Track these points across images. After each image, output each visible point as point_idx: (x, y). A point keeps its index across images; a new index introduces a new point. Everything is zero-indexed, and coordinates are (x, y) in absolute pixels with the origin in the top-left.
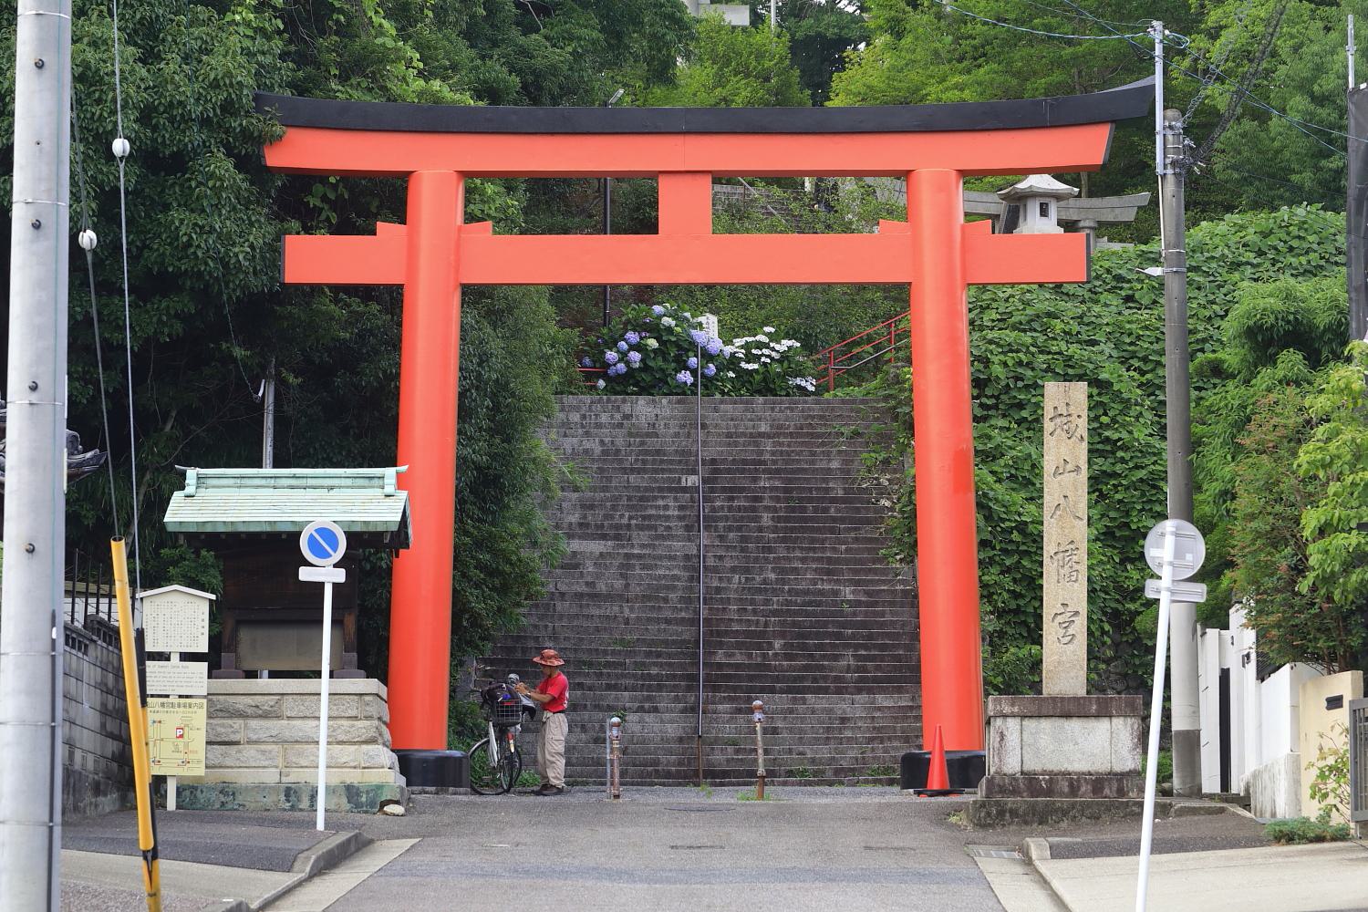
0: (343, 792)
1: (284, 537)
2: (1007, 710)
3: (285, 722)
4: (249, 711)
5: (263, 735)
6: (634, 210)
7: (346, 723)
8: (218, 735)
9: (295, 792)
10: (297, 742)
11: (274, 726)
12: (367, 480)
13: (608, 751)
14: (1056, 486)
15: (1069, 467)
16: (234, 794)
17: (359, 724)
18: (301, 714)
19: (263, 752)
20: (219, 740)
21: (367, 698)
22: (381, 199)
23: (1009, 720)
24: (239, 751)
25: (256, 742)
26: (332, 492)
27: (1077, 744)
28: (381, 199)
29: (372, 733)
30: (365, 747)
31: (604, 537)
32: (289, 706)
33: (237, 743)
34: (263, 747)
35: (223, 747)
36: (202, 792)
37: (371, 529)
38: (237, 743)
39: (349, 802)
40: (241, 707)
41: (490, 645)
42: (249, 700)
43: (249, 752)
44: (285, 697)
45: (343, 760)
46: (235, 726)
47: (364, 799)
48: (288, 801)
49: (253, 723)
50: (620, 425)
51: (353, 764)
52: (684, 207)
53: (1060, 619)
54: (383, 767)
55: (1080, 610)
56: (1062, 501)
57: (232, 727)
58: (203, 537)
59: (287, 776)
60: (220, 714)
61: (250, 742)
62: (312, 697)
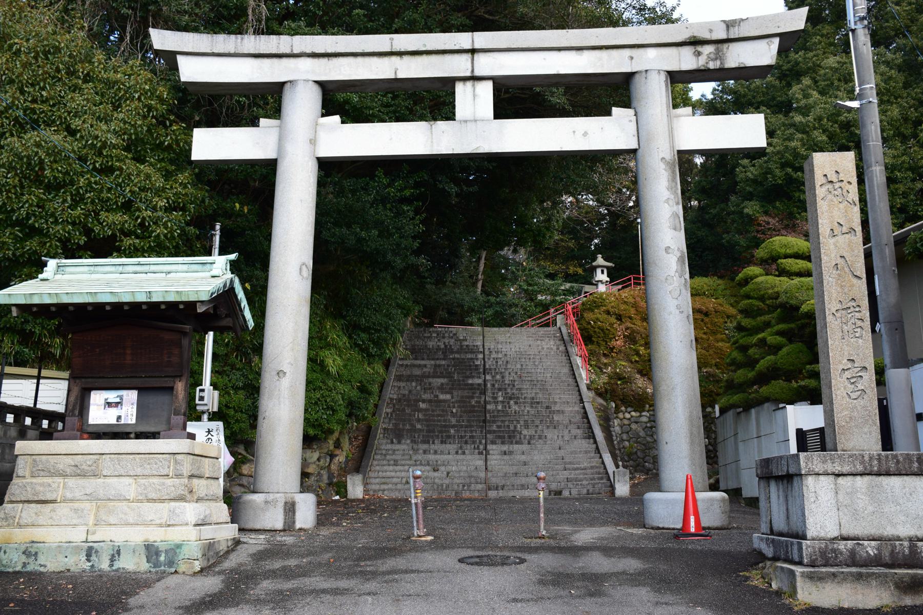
0: (143, 551)
1: (108, 308)
2: (819, 468)
3: (100, 481)
4: (68, 471)
5: (78, 494)
6: (431, 100)
7: (155, 480)
8: (36, 494)
9: (97, 552)
10: (109, 499)
11: (91, 485)
12: (200, 266)
13: (413, 496)
14: (832, 247)
15: (845, 229)
16: (36, 553)
17: (169, 482)
18: (116, 473)
19: (76, 511)
20: (36, 499)
21: (179, 457)
22: (254, 104)
23: (822, 478)
24: (53, 510)
25: (72, 500)
26: (169, 276)
27: (899, 504)
28: (254, 104)
29: (181, 491)
30: (173, 504)
31: (444, 377)
32: (107, 465)
33: (53, 501)
34: (76, 505)
35: (39, 506)
36: (5, 552)
37: (184, 299)
38: (53, 501)
39: (148, 562)
40: (61, 466)
41: (665, 507)
42: (69, 460)
43: (63, 510)
44: (104, 456)
45: (150, 518)
46: (54, 486)
47: (162, 558)
48: (89, 560)
49: (71, 482)
50: (452, 338)
51: (158, 522)
52: (474, 102)
53: (848, 374)
54: (187, 524)
55: (867, 366)
56: (840, 261)
57: (50, 485)
58: (35, 309)
59: (94, 533)
60: (42, 473)
61: (65, 501)
62: (131, 456)
